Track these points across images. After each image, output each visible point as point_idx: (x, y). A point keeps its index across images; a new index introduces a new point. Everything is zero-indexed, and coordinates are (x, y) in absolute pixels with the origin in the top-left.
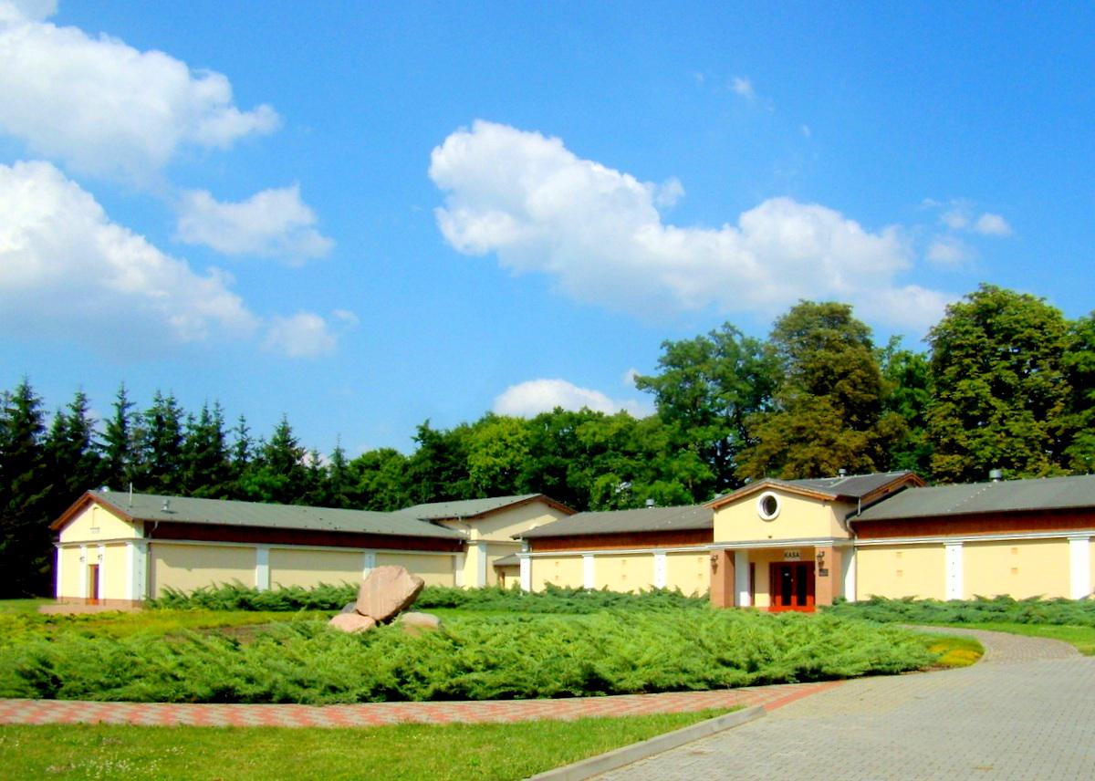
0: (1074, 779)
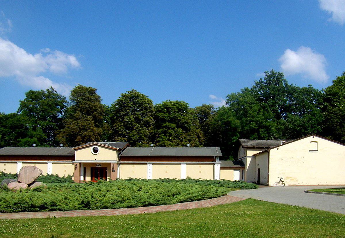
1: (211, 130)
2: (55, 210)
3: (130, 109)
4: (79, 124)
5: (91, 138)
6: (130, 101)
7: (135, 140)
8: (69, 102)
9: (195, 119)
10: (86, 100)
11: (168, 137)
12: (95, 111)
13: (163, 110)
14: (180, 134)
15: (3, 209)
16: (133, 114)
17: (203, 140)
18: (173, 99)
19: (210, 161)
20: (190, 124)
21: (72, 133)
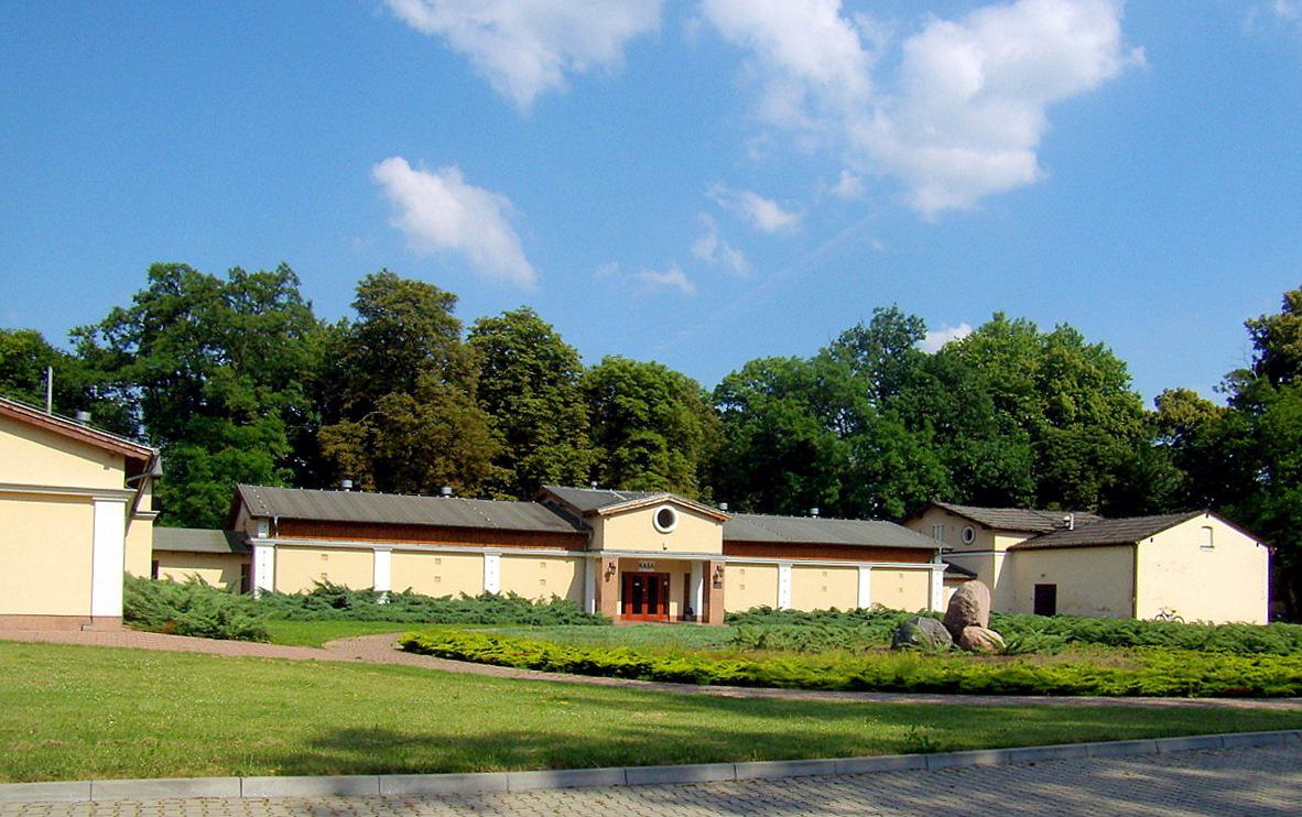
0: (244, 814)
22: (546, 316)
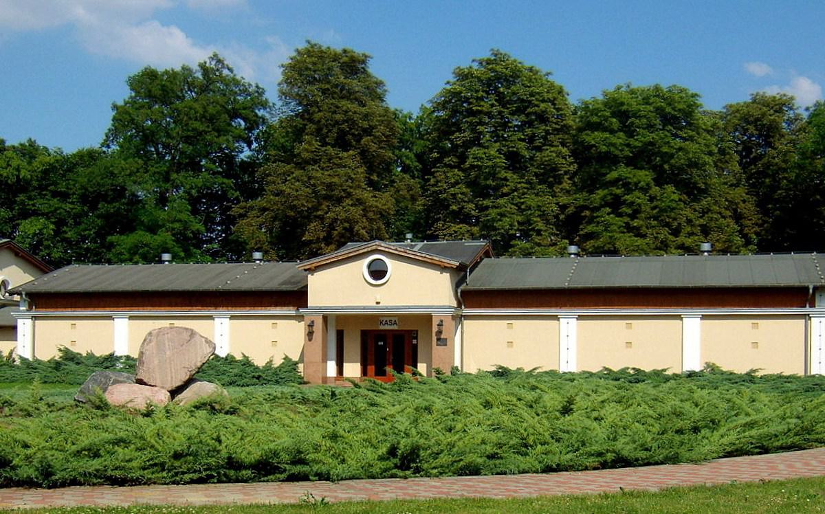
1: (787, 190)
2: (304, 477)
3: (487, 124)
4: (312, 182)
5: (356, 228)
6: (487, 93)
7: (507, 231)
8: (274, 104)
9: (722, 152)
10: (336, 96)
11: (627, 219)
12: (368, 131)
13: (606, 120)
14: (669, 207)
15: (141, 472)
16: (497, 137)
17: (757, 229)
18: (643, 82)
19: (792, 306)
20: (705, 171)
21: (292, 214)
22: (349, 47)
